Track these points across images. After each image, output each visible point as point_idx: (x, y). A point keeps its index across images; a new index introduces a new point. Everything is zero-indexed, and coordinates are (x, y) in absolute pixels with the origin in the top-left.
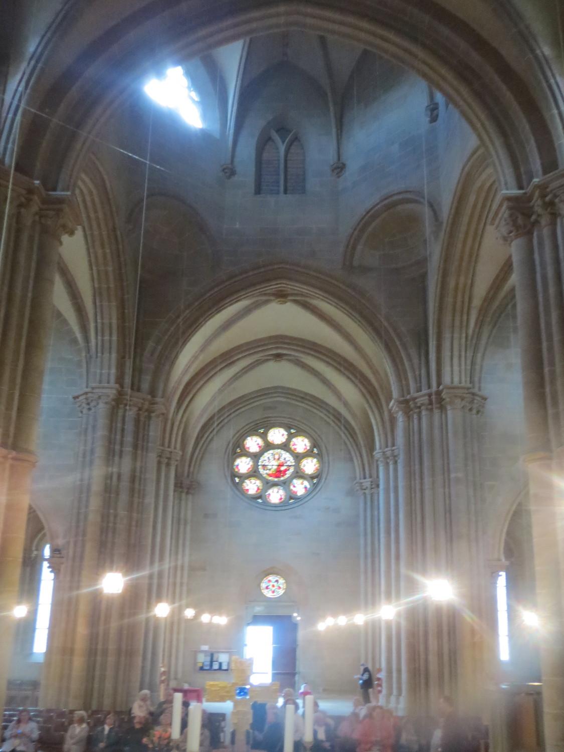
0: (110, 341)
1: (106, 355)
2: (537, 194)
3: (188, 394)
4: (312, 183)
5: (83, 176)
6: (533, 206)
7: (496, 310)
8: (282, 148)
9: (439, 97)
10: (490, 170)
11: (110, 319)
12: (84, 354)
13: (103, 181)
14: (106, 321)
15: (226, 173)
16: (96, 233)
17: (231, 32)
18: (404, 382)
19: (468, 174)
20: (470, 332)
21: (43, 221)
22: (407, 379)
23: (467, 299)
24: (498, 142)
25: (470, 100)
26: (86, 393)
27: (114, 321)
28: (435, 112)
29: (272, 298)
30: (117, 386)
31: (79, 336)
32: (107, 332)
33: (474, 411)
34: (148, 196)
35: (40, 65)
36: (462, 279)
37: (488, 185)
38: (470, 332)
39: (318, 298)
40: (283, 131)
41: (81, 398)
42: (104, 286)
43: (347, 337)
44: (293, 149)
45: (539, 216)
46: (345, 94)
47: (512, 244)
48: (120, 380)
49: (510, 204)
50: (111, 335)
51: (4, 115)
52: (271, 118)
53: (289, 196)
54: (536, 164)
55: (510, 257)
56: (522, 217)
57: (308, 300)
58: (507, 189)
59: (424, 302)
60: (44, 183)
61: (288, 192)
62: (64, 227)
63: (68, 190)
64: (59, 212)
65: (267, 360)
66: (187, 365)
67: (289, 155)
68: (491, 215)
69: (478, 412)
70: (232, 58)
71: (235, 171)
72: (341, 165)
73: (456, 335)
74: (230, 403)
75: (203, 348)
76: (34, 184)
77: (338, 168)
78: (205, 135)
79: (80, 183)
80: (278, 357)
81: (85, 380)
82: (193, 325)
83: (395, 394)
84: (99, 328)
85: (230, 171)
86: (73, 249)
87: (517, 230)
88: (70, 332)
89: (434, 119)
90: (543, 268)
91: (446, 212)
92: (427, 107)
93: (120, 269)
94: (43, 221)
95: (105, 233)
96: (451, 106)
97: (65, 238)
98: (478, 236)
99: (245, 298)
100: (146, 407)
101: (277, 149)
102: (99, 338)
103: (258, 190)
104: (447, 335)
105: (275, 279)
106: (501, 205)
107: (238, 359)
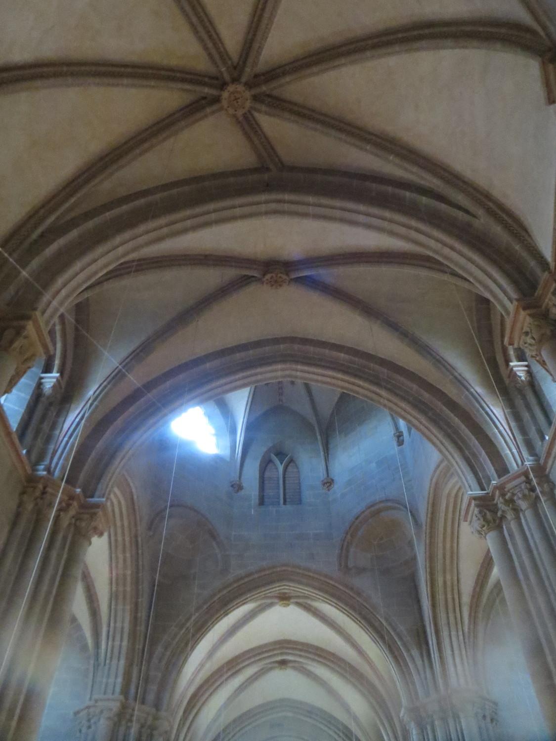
0: (120, 646)
1: (115, 662)
2: (497, 493)
3: (193, 707)
4: (307, 495)
5: (116, 490)
6: (497, 503)
7: (484, 602)
8: (281, 468)
9: (402, 423)
10: (455, 479)
11: (123, 622)
12: (92, 662)
13: (131, 493)
14: (119, 625)
15: (234, 488)
16: (120, 539)
17: (241, 382)
18: (411, 686)
19: (437, 484)
20: (466, 630)
21: (78, 523)
22: (413, 683)
23: (456, 597)
24: (457, 456)
25: (427, 424)
26: (88, 707)
27: (127, 626)
28: (401, 438)
29: (276, 601)
30: (122, 697)
31: (90, 641)
32: (118, 637)
33: (488, 720)
34: (171, 506)
35: (95, 403)
36: (448, 577)
37: (454, 492)
38: (466, 630)
39: (319, 599)
40: (280, 454)
41: (82, 714)
42: (121, 589)
43: (348, 638)
44: (290, 469)
45: (503, 511)
46: (330, 426)
47: (487, 537)
48: (125, 691)
49: (477, 502)
50: (121, 640)
51: (61, 439)
52: (271, 445)
53: (289, 507)
54: (491, 470)
55: (489, 551)
56: (490, 511)
57: (309, 602)
58: (471, 491)
59: (418, 601)
60: (84, 491)
61: (287, 503)
62: (95, 529)
63: (103, 497)
64: (93, 515)
65: (271, 669)
66: (193, 674)
67: (287, 473)
68: (463, 513)
69: (492, 720)
70: (240, 402)
71: (243, 486)
72: (330, 481)
73: (453, 633)
74: (235, 721)
75: (211, 654)
76: (75, 492)
77: (328, 482)
78: (218, 459)
79: (112, 496)
80: (283, 663)
81: (89, 691)
82: (202, 629)
83: (404, 701)
84: (111, 633)
85: (237, 487)
86: (98, 553)
87: (488, 525)
88: (82, 638)
89: (400, 443)
90: (519, 557)
91: (423, 517)
92: (394, 434)
93: (137, 573)
94: (78, 523)
95: (127, 539)
96: (413, 430)
97: (95, 540)
98: (455, 537)
99: (251, 600)
100: (149, 723)
101: (277, 468)
102: (110, 643)
103: (262, 502)
104: (445, 633)
105: (279, 581)
106: (469, 505)
107: (244, 667)
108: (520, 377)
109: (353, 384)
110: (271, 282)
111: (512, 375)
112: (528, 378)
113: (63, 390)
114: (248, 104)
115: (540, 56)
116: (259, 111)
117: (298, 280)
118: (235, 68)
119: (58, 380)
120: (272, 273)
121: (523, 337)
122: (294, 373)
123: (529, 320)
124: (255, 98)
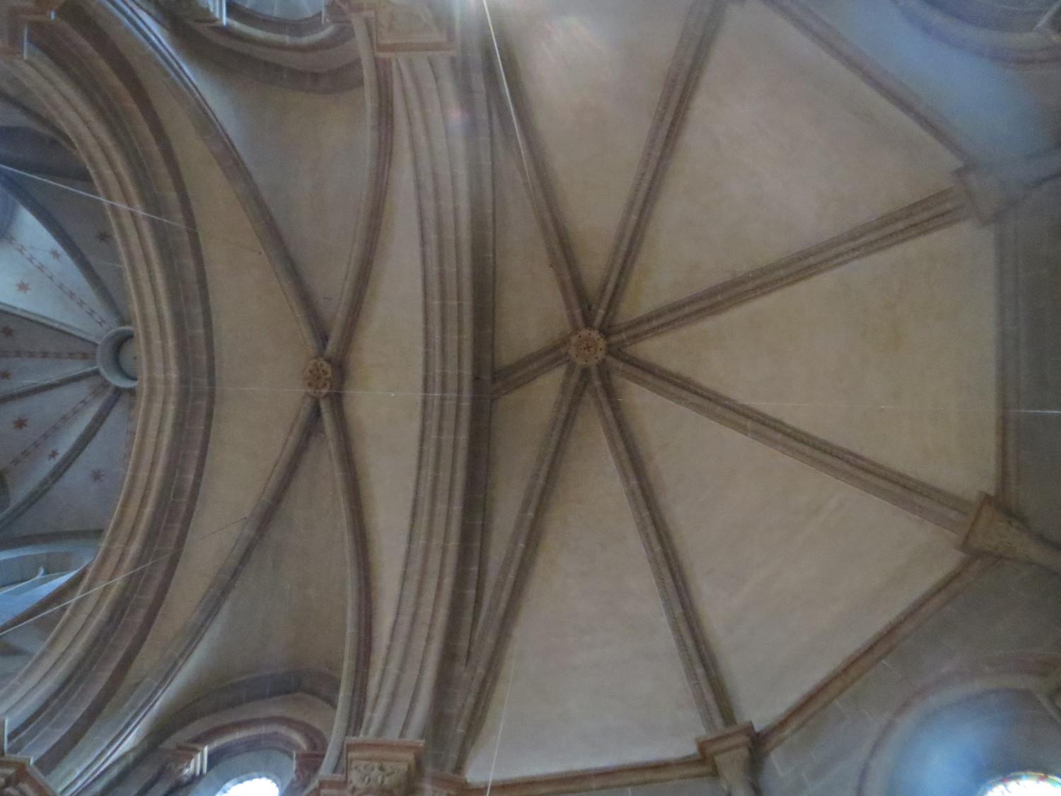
108: (188, 766)
109: (144, 498)
110: (318, 369)
111: (187, 752)
112: (185, 779)
113: (190, 22)
114: (580, 362)
115: (758, 734)
116: (569, 374)
117: (316, 412)
118: (619, 350)
119: (215, 20)
120: (333, 373)
121: (376, 765)
122: (160, 398)
123: (403, 767)
124: (585, 371)
